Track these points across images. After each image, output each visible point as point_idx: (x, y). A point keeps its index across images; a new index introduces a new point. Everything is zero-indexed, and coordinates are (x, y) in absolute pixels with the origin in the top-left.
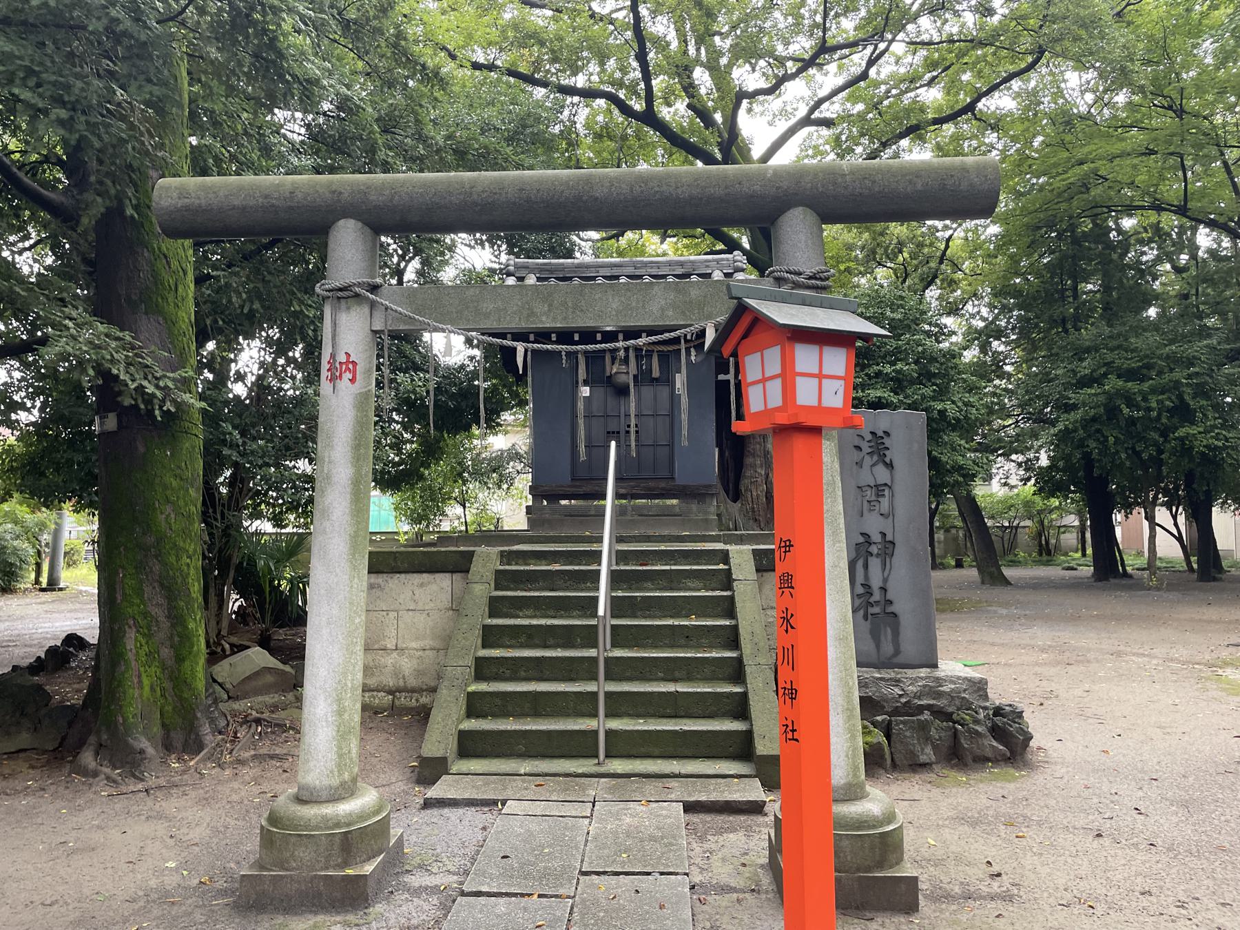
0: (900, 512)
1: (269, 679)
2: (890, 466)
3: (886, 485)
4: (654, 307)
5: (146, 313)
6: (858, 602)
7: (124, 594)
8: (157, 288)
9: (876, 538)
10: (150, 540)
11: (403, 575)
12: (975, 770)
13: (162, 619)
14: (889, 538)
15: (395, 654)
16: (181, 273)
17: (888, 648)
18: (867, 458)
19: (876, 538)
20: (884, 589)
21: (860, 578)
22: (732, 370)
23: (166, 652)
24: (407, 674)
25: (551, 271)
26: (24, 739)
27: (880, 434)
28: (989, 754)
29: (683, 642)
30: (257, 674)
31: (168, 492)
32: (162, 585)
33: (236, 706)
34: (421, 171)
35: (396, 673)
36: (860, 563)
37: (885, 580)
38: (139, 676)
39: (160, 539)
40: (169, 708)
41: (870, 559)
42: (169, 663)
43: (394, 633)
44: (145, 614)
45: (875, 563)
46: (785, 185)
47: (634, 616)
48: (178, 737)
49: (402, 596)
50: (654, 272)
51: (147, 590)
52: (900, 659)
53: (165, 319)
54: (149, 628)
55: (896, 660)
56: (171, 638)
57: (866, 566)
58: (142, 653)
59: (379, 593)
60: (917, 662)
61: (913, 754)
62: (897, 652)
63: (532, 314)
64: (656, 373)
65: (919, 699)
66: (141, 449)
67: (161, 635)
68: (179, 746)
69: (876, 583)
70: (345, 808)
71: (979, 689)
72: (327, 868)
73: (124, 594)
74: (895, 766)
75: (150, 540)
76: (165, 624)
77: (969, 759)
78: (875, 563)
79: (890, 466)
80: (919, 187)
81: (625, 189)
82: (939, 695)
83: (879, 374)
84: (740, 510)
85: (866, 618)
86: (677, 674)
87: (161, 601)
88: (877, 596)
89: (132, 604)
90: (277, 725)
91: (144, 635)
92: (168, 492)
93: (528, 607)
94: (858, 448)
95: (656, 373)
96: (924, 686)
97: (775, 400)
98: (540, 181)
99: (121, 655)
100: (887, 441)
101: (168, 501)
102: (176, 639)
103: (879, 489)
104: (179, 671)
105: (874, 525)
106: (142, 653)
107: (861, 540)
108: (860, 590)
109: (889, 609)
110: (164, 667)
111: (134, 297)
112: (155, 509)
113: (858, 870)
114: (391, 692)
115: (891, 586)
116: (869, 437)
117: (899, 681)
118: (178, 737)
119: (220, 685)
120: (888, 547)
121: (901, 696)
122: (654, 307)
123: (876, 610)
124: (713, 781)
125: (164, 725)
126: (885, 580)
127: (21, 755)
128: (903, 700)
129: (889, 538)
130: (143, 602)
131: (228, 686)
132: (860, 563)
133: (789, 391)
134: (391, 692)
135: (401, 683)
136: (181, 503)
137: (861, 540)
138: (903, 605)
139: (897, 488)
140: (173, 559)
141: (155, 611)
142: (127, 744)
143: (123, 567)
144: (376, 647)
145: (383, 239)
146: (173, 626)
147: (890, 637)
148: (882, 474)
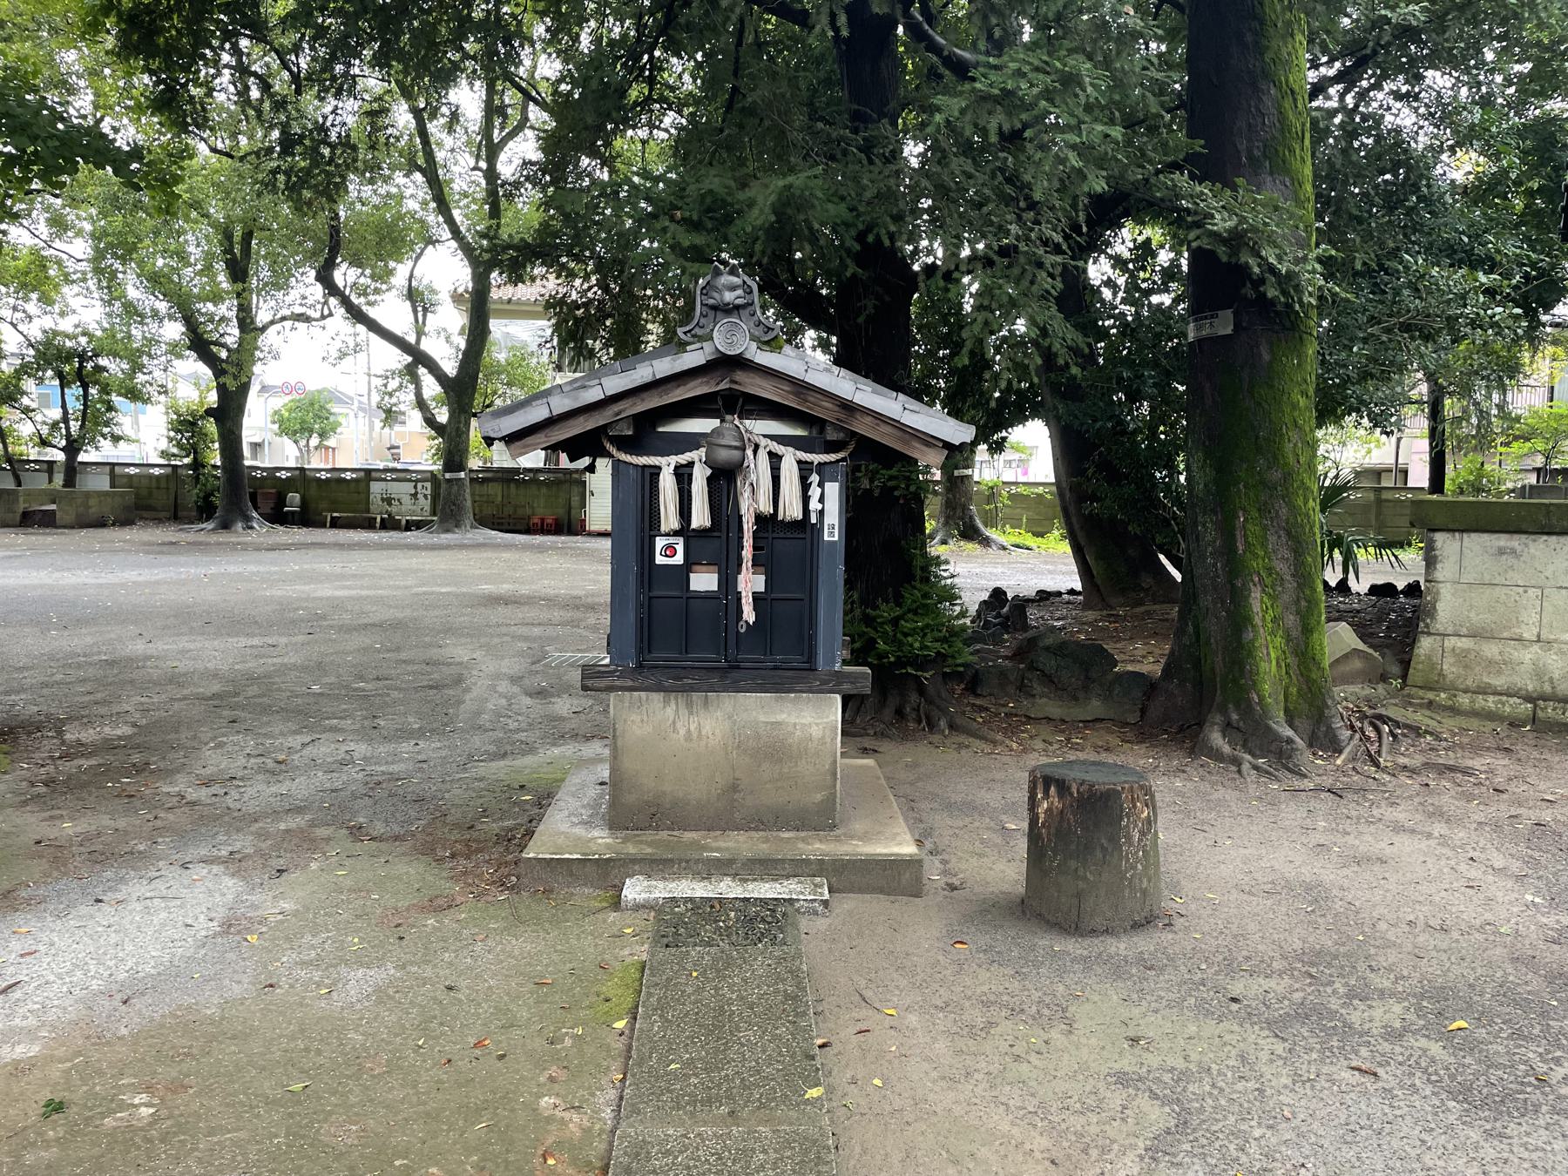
1: (1357, 664)
5: (1271, 174)
7: (1248, 544)
8: (1284, 138)
10: (1276, 475)
11: (1554, 538)
15: (1536, 648)
22: (724, 528)
23: (1291, 619)
24: (1556, 676)
26: (1096, 707)
30: (1346, 656)
32: (1289, 533)
35: (1539, 673)
39: (1288, 476)
40: (1294, 690)
42: (1294, 634)
43: (1535, 618)
44: (1270, 570)
49: (1551, 568)
51: (1272, 539)
53: (1292, 180)
56: (1297, 602)
58: (1268, 619)
59: (1511, 561)
66: (1266, 357)
73: (1248, 544)
75: (1276, 475)
76: (1291, 584)
89: (1256, 556)
90: (1407, 726)
92: (1296, 414)
99: (1248, 619)
102: (1303, 603)
104: (1307, 645)
106: (1268, 619)
110: (1288, 638)
111: (1256, 152)
112: (1282, 435)
114: (1529, 699)
127: (1098, 725)
134: (1529, 699)
135: (1547, 688)
140: (1300, 502)
142: (1269, 728)
143: (1244, 510)
144: (1505, 635)
145: (968, 308)
146: (1300, 587)
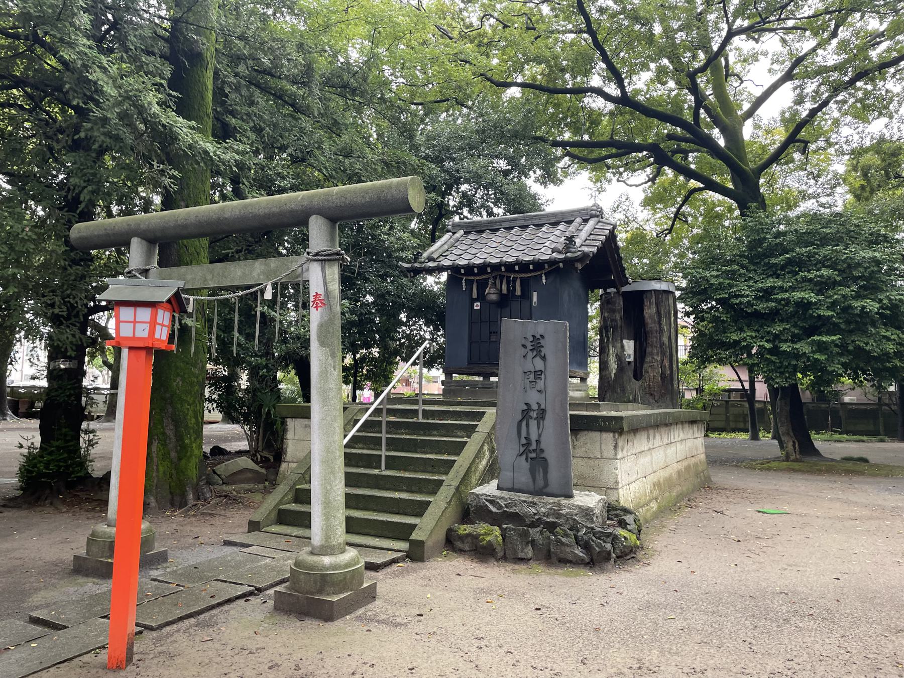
0: (549, 390)
1: (250, 475)
2: (544, 358)
3: (541, 371)
4: (255, 274)
6: (522, 449)
9: (535, 407)
12: (557, 567)
13: (172, 436)
14: (543, 407)
16: (196, 254)
17: (540, 482)
18: (530, 353)
19: (535, 407)
20: (538, 442)
21: (524, 434)
23: (173, 454)
25: (473, 227)
27: (538, 336)
28: (570, 557)
29: (430, 469)
31: (179, 371)
33: (225, 487)
34: (187, 207)
36: (524, 423)
37: (540, 436)
38: (157, 466)
41: (530, 421)
44: (164, 434)
45: (533, 424)
46: (305, 204)
47: (416, 452)
48: (177, 499)
50: (536, 222)
52: (548, 490)
54: (165, 441)
55: (545, 491)
57: (527, 425)
60: (559, 493)
61: (515, 552)
62: (546, 485)
63: (206, 280)
64: (518, 293)
65: (547, 517)
67: (171, 445)
68: (177, 504)
69: (534, 437)
70: (327, 560)
71: (587, 515)
72: (102, 557)
74: (505, 558)
75: (168, 395)
77: (554, 559)
78: (533, 424)
79: (544, 358)
80: (367, 199)
81: (276, 210)
82: (559, 516)
83: (805, 280)
84: (640, 387)
85: (527, 459)
86: (413, 488)
87: (171, 427)
88: (534, 446)
91: (162, 445)
92: (179, 371)
93: (360, 442)
94: (524, 346)
95: (518, 293)
96: (551, 509)
97: (145, 334)
98: (290, 200)
100: (542, 341)
101: (178, 375)
103: (538, 374)
105: (534, 398)
107: (525, 407)
108: (524, 441)
109: (543, 456)
110: (172, 462)
113: (307, 593)
115: (543, 439)
116: (531, 339)
117: (535, 504)
118: (177, 499)
119: (219, 476)
120: (542, 413)
121: (535, 514)
122: (255, 274)
123: (533, 455)
124: (378, 551)
125: (171, 493)
126: (540, 436)
128: (537, 517)
129: (543, 407)
130: (163, 427)
131: (223, 477)
132: (524, 423)
133: (152, 331)
136: (186, 376)
137: (525, 407)
138: (551, 454)
139: (549, 373)
140: (179, 406)
141: (168, 432)
146: (177, 441)
147: (541, 474)
148: (539, 364)
